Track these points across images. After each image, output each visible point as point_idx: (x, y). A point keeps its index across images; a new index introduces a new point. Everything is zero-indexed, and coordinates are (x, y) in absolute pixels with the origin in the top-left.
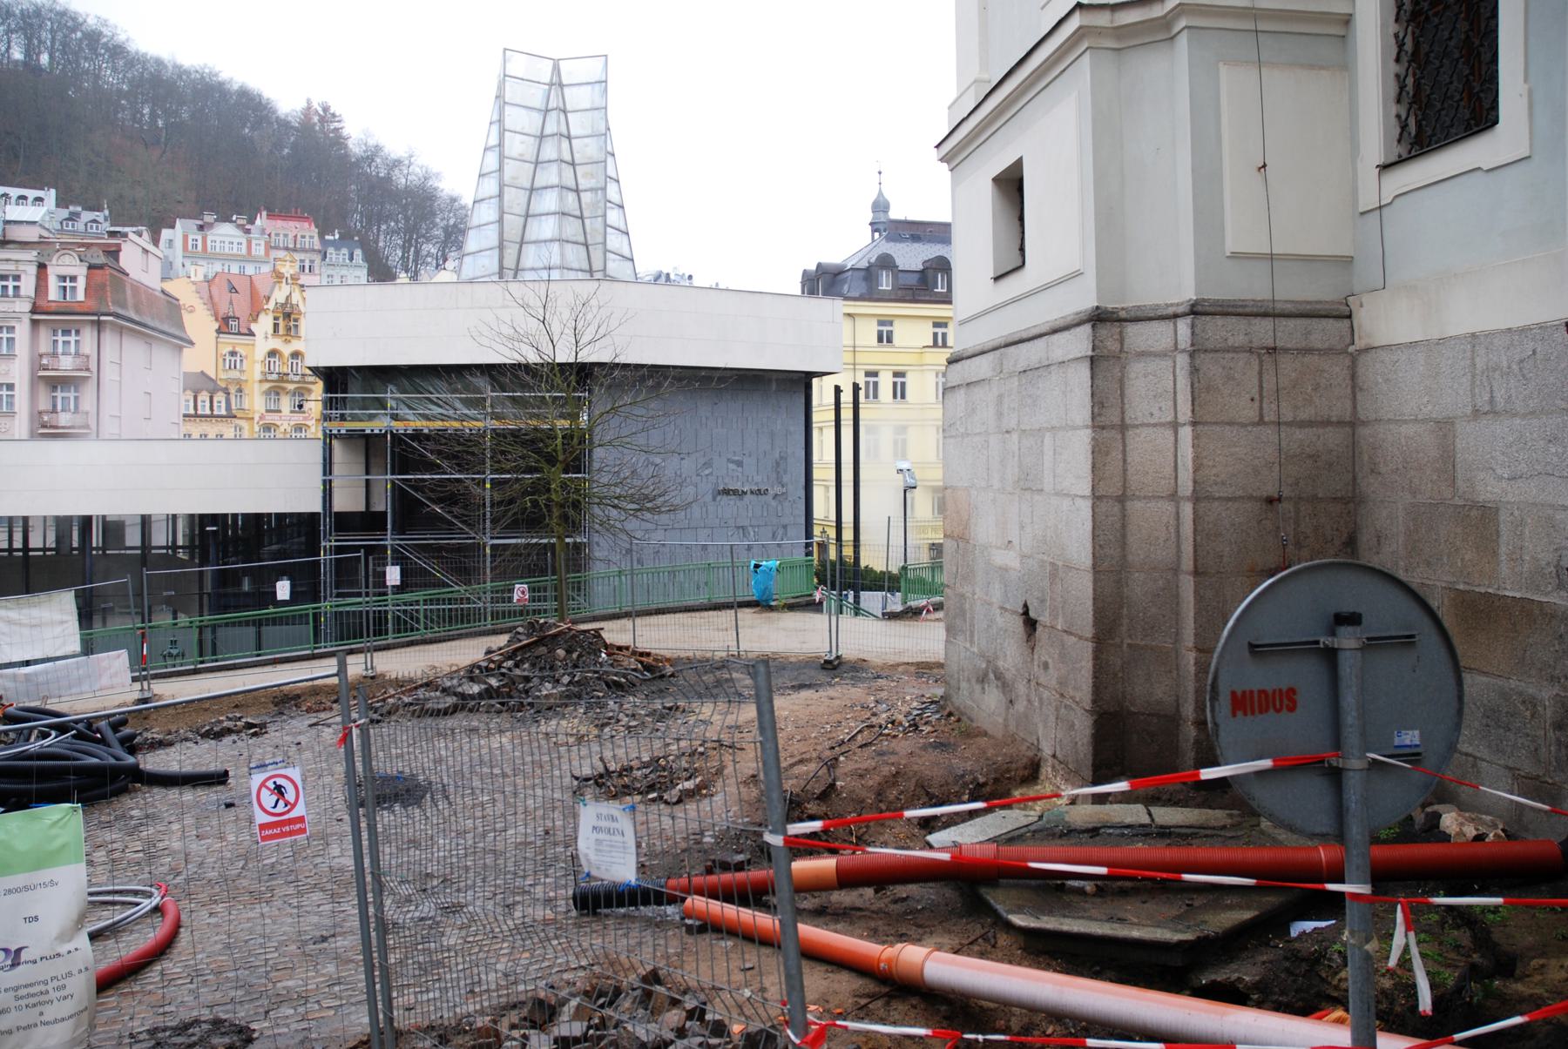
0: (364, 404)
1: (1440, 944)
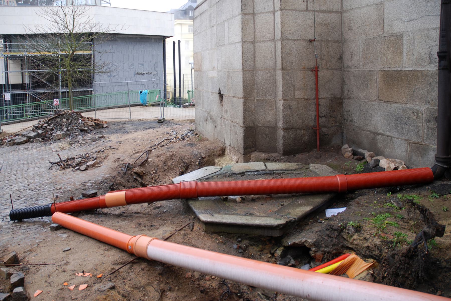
0: (18, 46)
1: (395, 217)
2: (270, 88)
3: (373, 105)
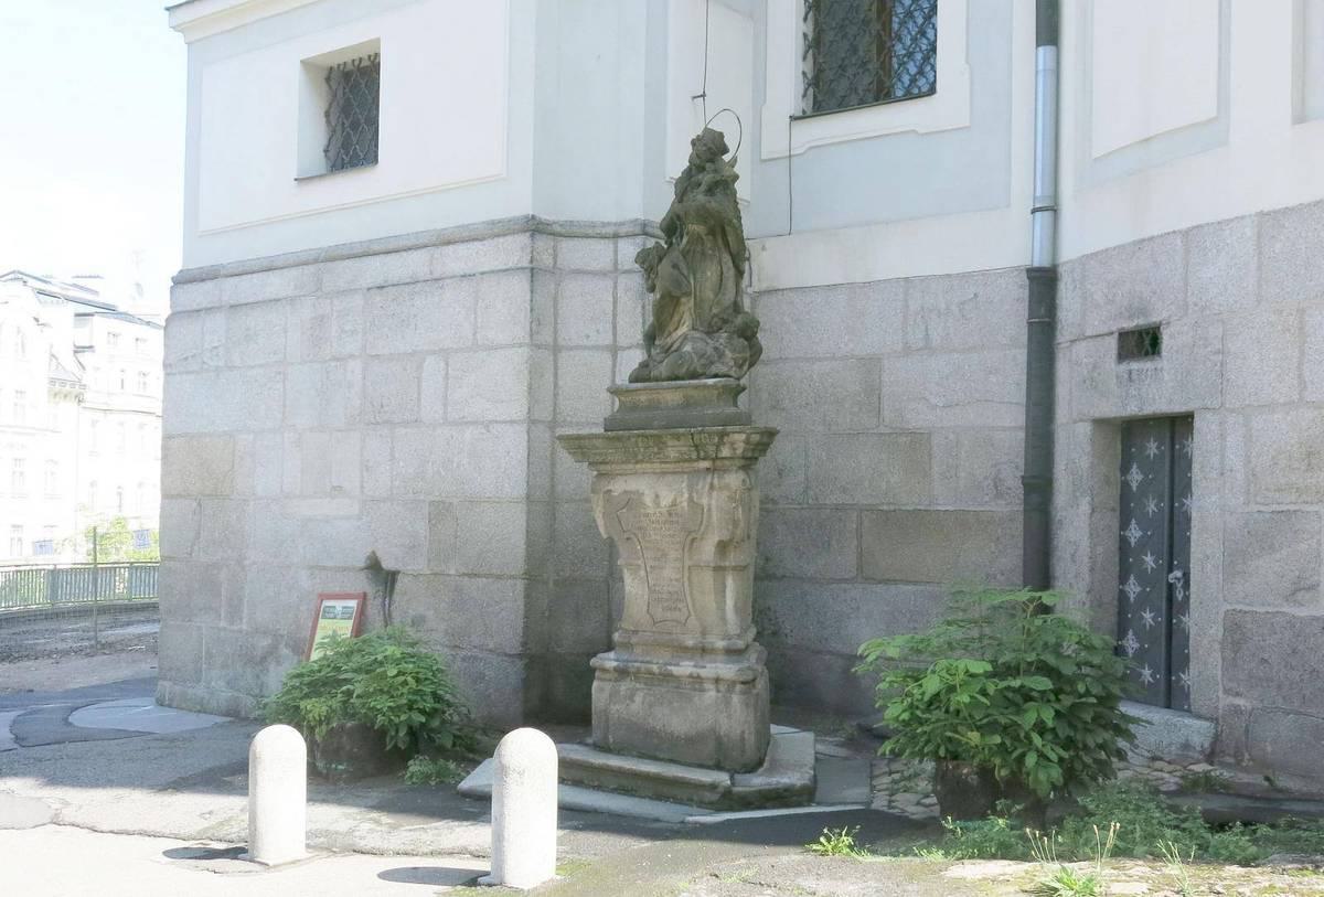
3: (845, 591)
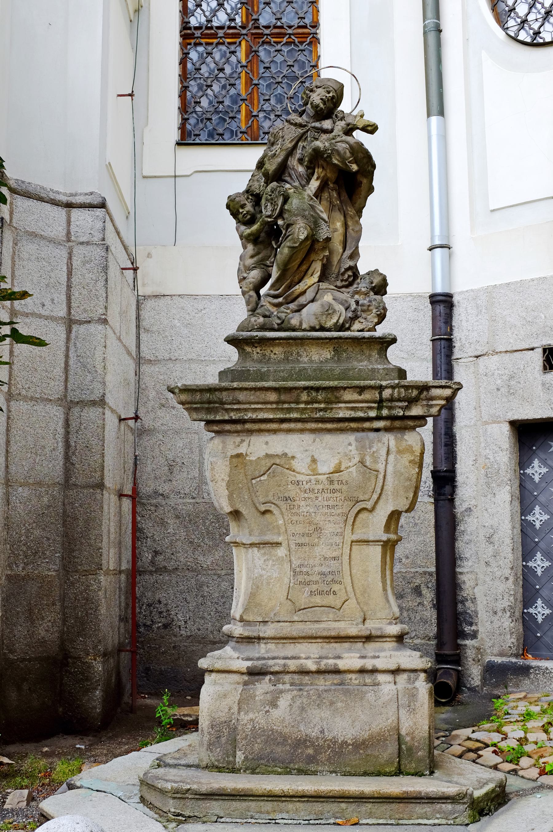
2: (48, 539)
